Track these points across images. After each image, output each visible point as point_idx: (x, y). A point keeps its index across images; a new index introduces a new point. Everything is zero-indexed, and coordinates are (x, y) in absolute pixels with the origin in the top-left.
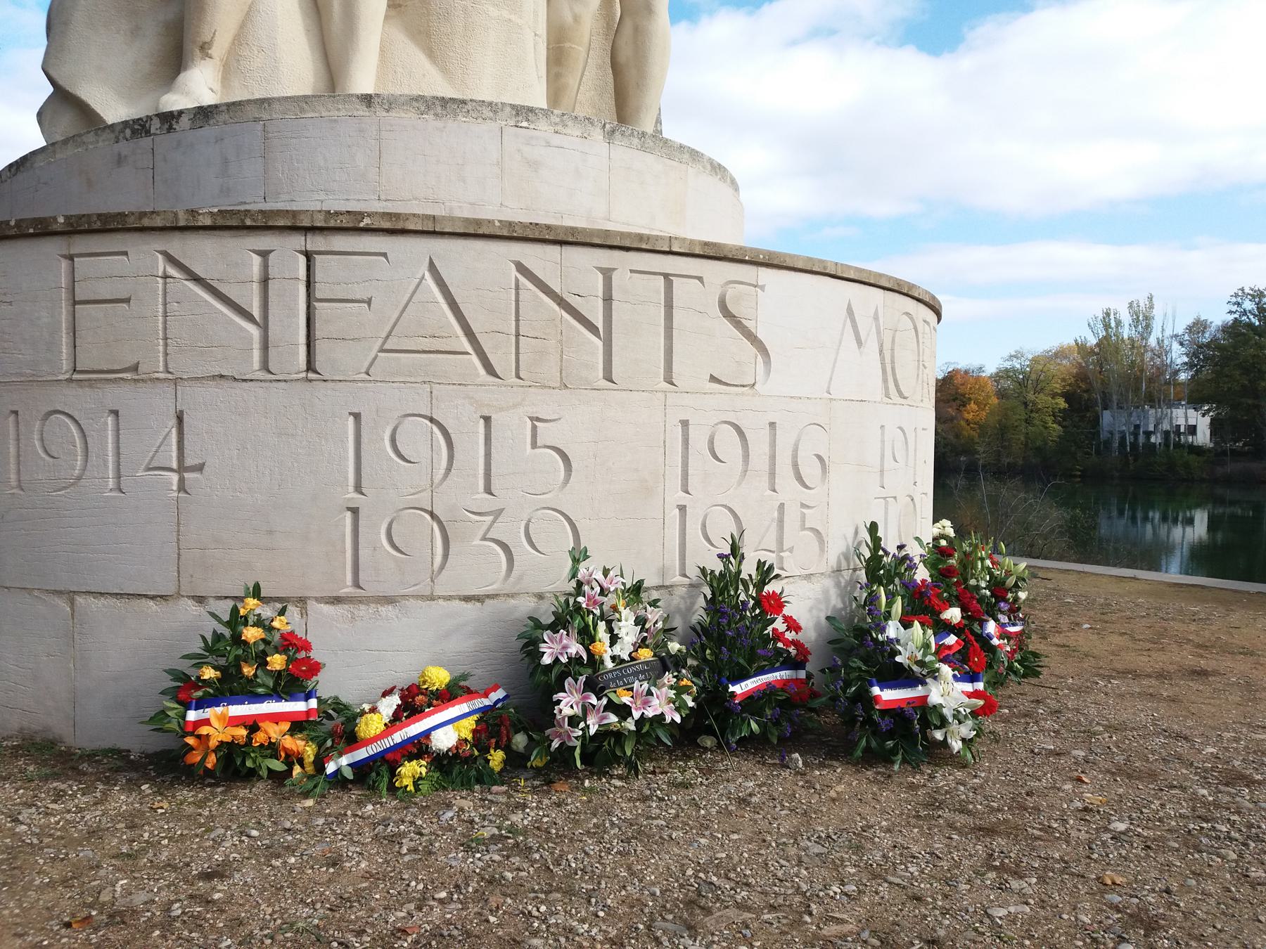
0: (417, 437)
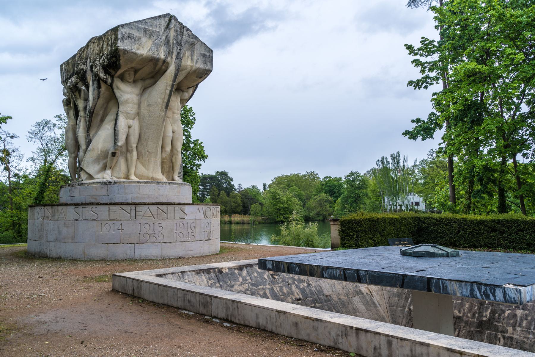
0: (146, 226)
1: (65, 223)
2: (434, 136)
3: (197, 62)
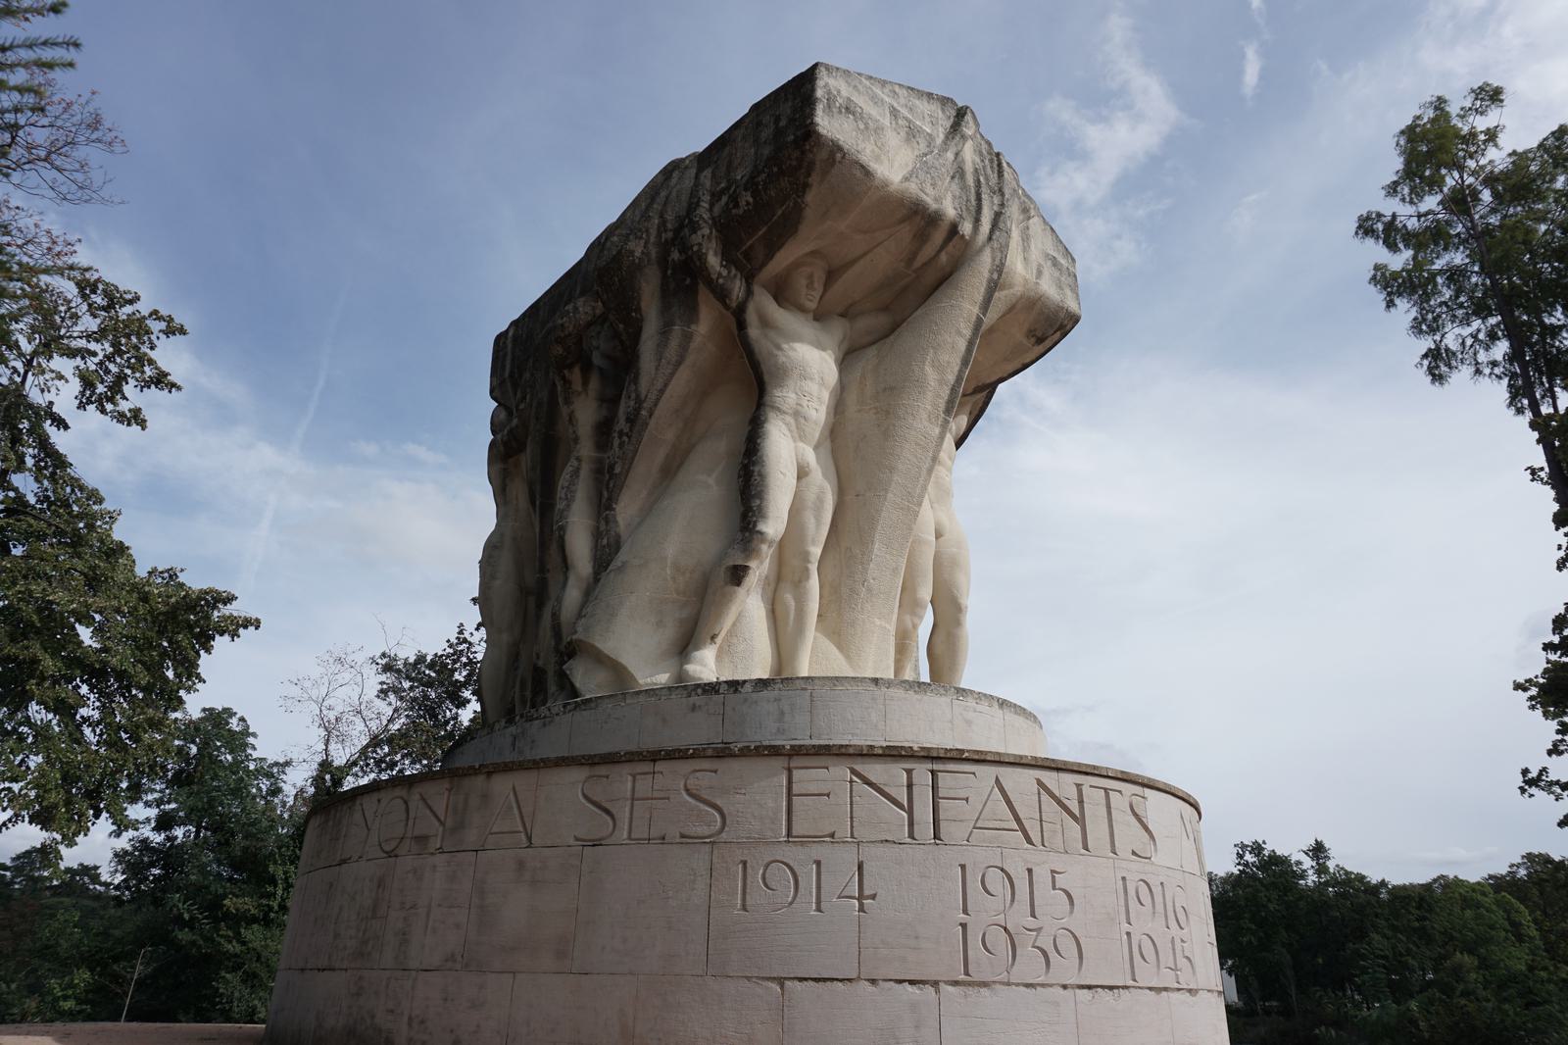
0: (995, 879)
1: (521, 864)
2: (1313, 842)
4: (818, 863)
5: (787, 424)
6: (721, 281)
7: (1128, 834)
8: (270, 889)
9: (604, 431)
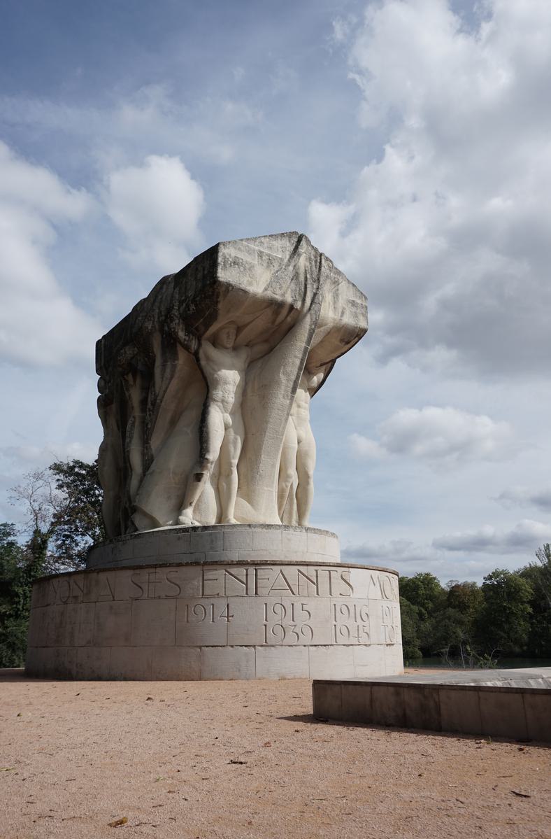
0: (279, 609)
1: (111, 608)
3: (343, 313)
4: (213, 605)
5: (218, 406)
6: (186, 342)
7: (339, 586)
8: (16, 600)
9: (144, 402)
